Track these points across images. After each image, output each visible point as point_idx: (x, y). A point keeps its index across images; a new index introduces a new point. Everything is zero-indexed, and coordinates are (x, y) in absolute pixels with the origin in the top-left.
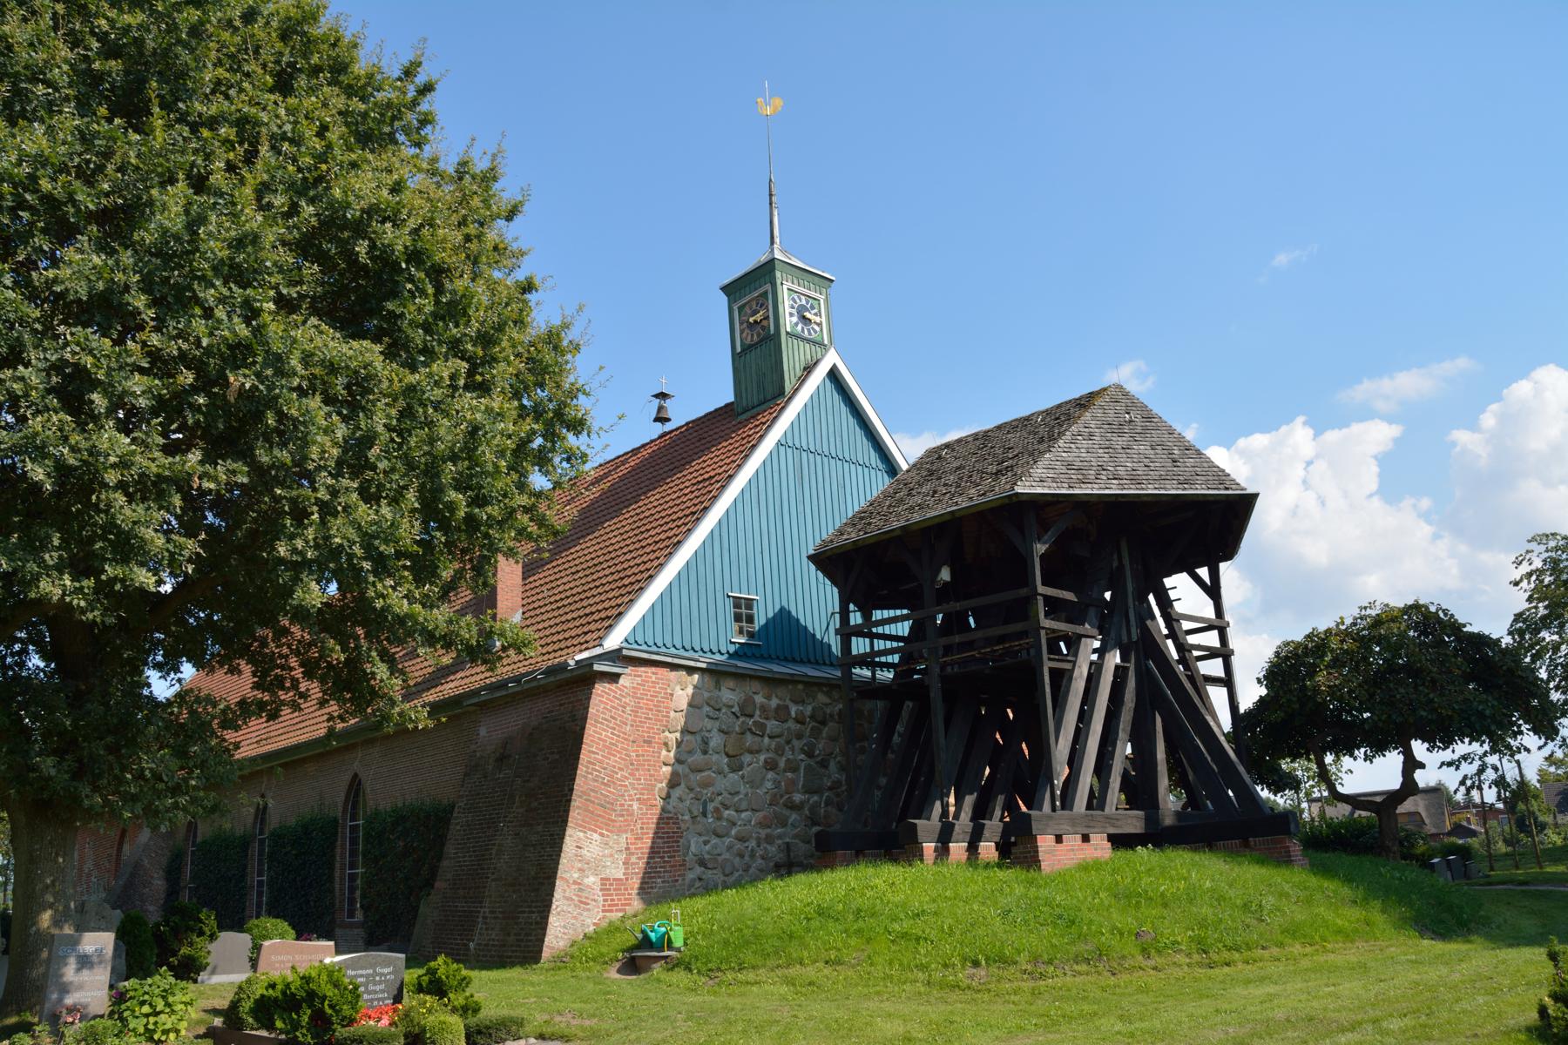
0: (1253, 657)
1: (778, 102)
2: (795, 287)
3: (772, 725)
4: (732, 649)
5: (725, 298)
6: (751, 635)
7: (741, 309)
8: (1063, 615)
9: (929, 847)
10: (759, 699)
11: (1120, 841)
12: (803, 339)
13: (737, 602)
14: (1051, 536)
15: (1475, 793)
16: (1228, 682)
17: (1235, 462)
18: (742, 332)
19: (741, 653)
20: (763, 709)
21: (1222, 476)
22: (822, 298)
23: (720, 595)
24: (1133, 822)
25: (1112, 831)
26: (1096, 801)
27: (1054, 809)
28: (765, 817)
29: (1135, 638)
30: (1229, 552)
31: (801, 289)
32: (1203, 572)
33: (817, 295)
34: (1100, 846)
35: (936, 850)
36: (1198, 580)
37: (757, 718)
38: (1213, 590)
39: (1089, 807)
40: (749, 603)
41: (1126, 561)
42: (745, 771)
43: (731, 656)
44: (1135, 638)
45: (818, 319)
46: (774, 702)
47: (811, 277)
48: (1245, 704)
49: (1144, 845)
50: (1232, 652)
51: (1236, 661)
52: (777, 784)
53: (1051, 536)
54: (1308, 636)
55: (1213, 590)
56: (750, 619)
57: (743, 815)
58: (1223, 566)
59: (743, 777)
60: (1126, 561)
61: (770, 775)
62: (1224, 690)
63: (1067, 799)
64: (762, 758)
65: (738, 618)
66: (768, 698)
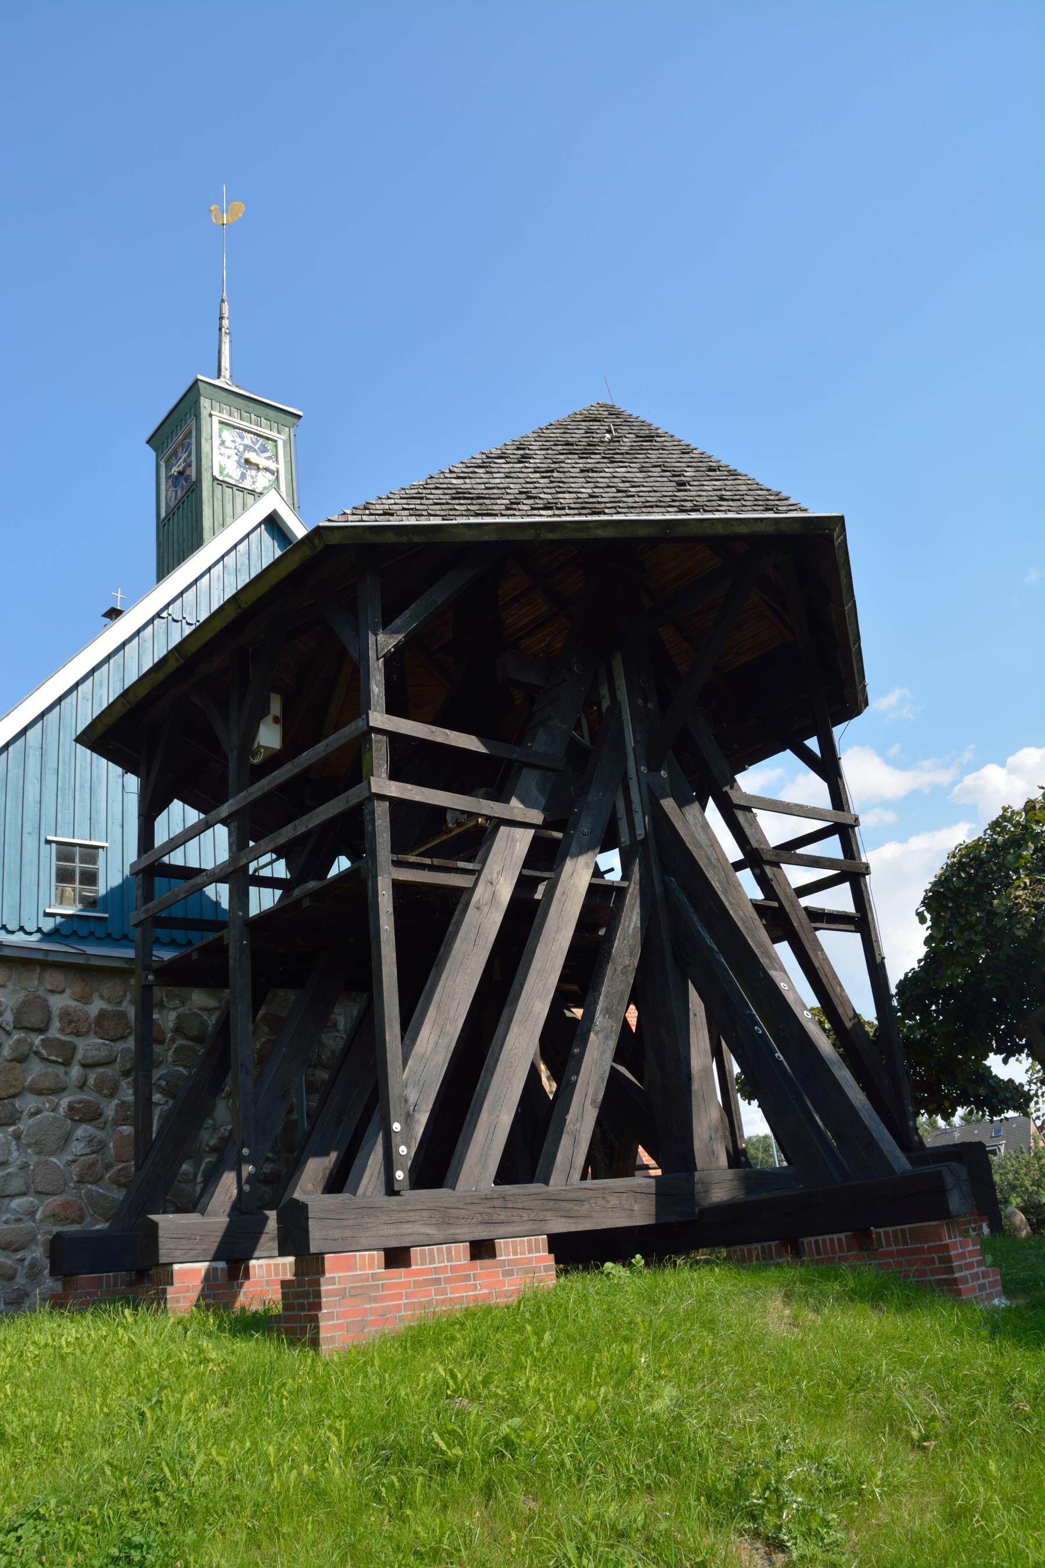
0: (903, 875)
1: (240, 207)
2: (225, 417)
3: (89, 1046)
4: (48, 925)
5: (154, 453)
6: (91, 903)
7: (167, 462)
8: (482, 791)
9: (190, 1274)
10: (58, 1003)
11: (575, 1251)
12: (241, 490)
13: (65, 851)
14: (408, 620)
15: (785, 1320)
16: (860, 921)
17: (784, 464)
18: (167, 491)
19: (67, 930)
20: (68, 1018)
21: (771, 500)
22: (281, 439)
23: (30, 844)
24: (624, 1203)
25: (561, 1226)
26: (527, 1156)
27: (391, 1189)
28: (66, 1205)
29: (640, 833)
30: (849, 700)
31: (245, 424)
32: (813, 744)
33: (273, 434)
34: (525, 1260)
35: (209, 1277)
36: (806, 756)
37: (55, 1031)
38: (828, 767)
39: (503, 1177)
40: (90, 853)
41: (623, 696)
42: (24, 1125)
43: (47, 936)
44: (640, 833)
45: (273, 466)
46: (96, 1007)
47: (272, 413)
48: (897, 970)
49: (623, 1258)
50: (866, 869)
51: (873, 883)
52: (99, 1147)
53: (408, 620)
54: (995, 825)
55: (828, 767)
56: (90, 878)
57: (15, 1203)
58: (837, 731)
59: (17, 1136)
60: (623, 696)
61: (82, 1130)
62: (855, 939)
63: (436, 1164)
64: (64, 1102)
65: (64, 876)
66: (86, 999)
